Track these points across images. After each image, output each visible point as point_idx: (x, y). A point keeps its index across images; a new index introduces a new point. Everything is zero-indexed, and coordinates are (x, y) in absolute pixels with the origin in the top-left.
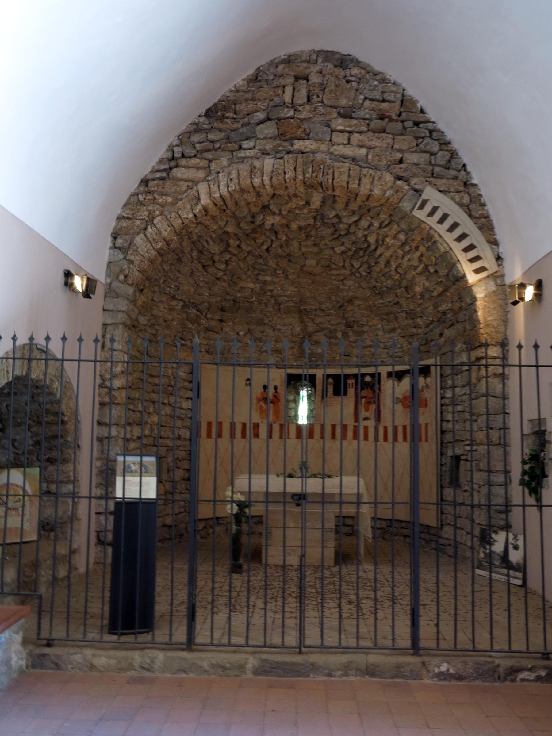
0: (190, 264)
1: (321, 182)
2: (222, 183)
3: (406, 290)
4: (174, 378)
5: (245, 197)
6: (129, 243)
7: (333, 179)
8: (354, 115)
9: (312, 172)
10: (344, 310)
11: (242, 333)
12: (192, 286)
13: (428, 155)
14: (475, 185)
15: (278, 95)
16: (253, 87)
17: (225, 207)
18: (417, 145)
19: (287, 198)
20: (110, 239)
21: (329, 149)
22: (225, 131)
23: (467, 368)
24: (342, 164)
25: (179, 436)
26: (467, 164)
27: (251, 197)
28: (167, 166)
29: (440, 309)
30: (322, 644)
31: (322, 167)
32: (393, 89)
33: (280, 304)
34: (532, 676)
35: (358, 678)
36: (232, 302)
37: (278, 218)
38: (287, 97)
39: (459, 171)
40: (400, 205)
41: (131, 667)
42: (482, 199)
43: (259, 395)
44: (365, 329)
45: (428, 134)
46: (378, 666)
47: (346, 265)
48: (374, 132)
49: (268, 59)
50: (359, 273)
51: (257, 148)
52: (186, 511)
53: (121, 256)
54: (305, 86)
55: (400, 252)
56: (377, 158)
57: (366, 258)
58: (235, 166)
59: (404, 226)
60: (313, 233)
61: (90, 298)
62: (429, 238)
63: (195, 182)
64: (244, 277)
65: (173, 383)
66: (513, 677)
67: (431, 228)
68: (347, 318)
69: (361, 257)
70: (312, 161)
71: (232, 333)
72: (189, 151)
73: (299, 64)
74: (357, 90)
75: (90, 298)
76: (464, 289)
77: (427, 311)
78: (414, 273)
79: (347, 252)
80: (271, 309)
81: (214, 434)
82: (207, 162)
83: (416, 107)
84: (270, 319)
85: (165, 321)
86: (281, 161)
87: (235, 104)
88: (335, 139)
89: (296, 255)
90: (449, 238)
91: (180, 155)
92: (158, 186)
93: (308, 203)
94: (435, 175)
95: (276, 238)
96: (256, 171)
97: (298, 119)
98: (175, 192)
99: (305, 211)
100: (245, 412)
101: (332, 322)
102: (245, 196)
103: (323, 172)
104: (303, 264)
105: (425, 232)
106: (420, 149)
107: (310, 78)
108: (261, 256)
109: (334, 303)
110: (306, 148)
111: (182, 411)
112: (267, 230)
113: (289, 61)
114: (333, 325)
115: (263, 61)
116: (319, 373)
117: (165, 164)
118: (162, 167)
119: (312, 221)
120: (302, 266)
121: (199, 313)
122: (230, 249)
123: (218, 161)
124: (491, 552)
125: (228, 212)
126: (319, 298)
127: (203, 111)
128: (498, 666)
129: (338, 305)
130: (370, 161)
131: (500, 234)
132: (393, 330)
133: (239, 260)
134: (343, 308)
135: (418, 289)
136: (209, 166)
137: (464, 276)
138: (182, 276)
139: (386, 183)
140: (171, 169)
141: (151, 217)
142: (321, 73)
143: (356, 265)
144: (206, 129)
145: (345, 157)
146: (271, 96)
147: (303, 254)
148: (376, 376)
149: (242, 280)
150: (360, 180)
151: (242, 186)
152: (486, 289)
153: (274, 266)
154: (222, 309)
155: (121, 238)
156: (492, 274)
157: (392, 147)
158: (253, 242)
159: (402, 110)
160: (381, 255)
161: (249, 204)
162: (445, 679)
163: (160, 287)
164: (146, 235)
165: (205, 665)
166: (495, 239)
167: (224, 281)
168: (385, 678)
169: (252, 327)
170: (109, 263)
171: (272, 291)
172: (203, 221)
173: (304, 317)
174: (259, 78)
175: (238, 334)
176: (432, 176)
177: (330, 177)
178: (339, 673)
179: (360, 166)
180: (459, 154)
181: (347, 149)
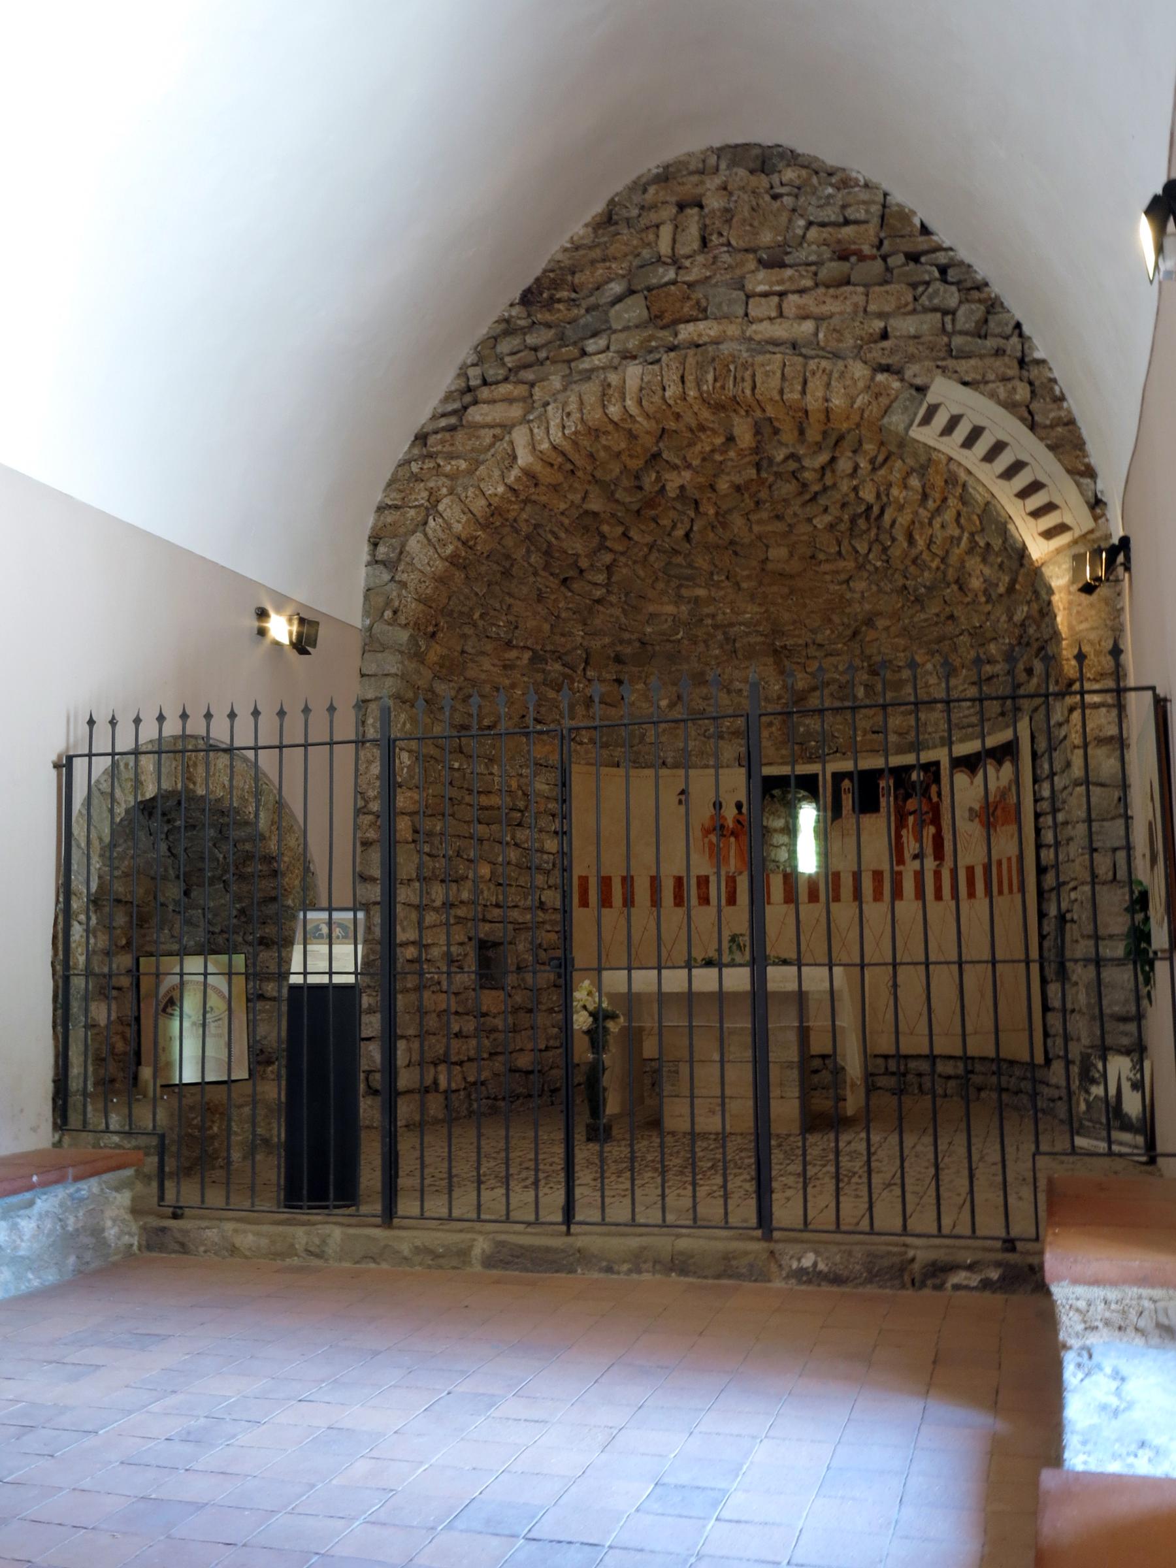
0: (532, 579)
1: (735, 397)
2: (552, 423)
4: (525, 794)
7: (754, 388)
8: (788, 260)
9: (715, 380)
12: (546, 620)
13: (939, 315)
15: (649, 244)
16: (603, 235)
17: (569, 467)
18: (915, 299)
20: (366, 548)
21: (743, 332)
22: (557, 326)
24: (768, 356)
25: (541, 903)
26: (1021, 321)
28: (457, 405)
32: (864, 195)
33: (735, 641)
34: (974, 1280)
35: (658, 1276)
36: (637, 644)
37: (687, 475)
38: (664, 247)
39: (1007, 338)
40: (885, 420)
41: (291, 1251)
42: (1057, 389)
43: (707, 823)
45: (937, 274)
46: (692, 1257)
47: (843, 552)
48: (828, 287)
49: (628, 180)
51: (612, 348)
53: (386, 577)
54: (696, 218)
58: (575, 387)
59: (910, 462)
60: (763, 494)
61: (308, 653)
62: (951, 480)
63: (507, 428)
65: (521, 804)
66: (938, 1281)
67: (950, 459)
68: (870, 657)
69: (865, 532)
70: (713, 360)
72: (494, 372)
73: (684, 180)
74: (794, 210)
75: (308, 653)
80: (717, 652)
82: (526, 387)
83: (911, 224)
84: (719, 671)
86: (656, 367)
87: (573, 273)
88: (753, 313)
91: (479, 382)
93: (731, 439)
94: (954, 353)
96: (611, 392)
97: (684, 283)
98: (472, 450)
99: (732, 454)
100: (681, 855)
102: (603, 440)
103: (735, 378)
104: (763, 557)
106: (923, 306)
107: (704, 202)
108: (676, 552)
109: (841, 628)
110: (700, 335)
111: (545, 857)
112: (674, 499)
113: (665, 177)
115: (618, 185)
117: (454, 400)
119: (753, 472)
122: (608, 544)
123: (545, 383)
125: (580, 474)
126: (807, 621)
127: (516, 295)
128: (913, 1260)
129: (849, 632)
130: (822, 344)
133: (635, 562)
134: (859, 638)
135: (976, 583)
136: (531, 395)
138: (518, 602)
139: (855, 382)
140: (465, 408)
141: (433, 499)
142: (725, 189)
143: (862, 548)
144: (522, 328)
145: (776, 343)
146: (636, 247)
147: (759, 537)
148: (932, 769)
151: (590, 424)
153: (705, 566)
154: (618, 659)
156: (1084, 536)
157: (865, 311)
158: (653, 525)
159: (882, 235)
160: (894, 522)
161: (618, 454)
162: (809, 1282)
163: (475, 625)
164: (426, 535)
165: (405, 1248)
168: (705, 1277)
170: (368, 590)
171: (713, 616)
172: (534, 497)
173: (786, 663)
174: (615, 217)
176: (947, 356)
178: (625, 1267)
179: (805, 357)
180: (1006, 304)
181: (776, 327)
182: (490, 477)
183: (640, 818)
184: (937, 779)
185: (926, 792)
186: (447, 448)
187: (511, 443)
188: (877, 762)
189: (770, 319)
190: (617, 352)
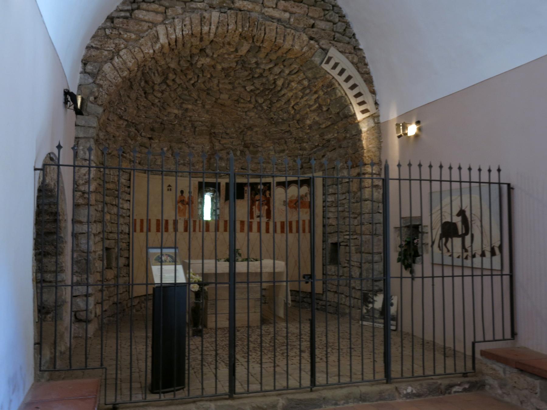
2: (177, 27)
3: (297, 122)
5: (192, 40)
6: (98, 69)
7: (265, 34)
10: (244, 134)
11: (165, 149)
14: (361, 50)
18: (324, 15)
19: (222, 45)
20: (80, 65)
21: (261, 10)
23: (347, 180)
24: (271, 23)
27: (196, 41)
28: (129, 8)
29: (326, 137)
30: (327, 383)
31: (256, 23)
35: (355, 404)
39: (350, 38)
40: (313, 59)
42: (366, 61)
44: (260, 149)
45: (331, 8)
50: (262, 107)
52: (126, 291)
55: (300, 94)
56: (297, 21)
57: (270, 96)
58: (188, 14)
60: (232, 74)
63: (155, 24)
64: (172, 104)
67: (333, 78)
70: (249, 18)
71: (158, 149)
76: (352, 124)
77: (314, 138)
78: (308, 110)
79: (255, 90)
81: (145, 229)
84: (187, 139)
85: (114, 137)
86: (226, 15)
89: (215, 90)
90: (346, 86)
92: (123, 23)
93: (236, 51)
95: (203, 76)
96: (205, 20)
98: (138, 30)
99: (232, 56)
101: (234, 144)
105: (328, 81)
106: (326, 18)
111: (124, 211)
112: (197, 68)
114: (235, 145)
116: (223, 182)
117: (128, 5)
118: (126, 8)
120: (217, 99)
121: (136, 132)
122: (168, 81)
123: (174, 9)
124: (373, 308)
128: (441, 384)
129: (240, 130)
131: (377, 86)
132: (283, 151)
134: (244, 133)
136: (165, 12)
137: (355, 114)
139: (303, 41)
140: (133, 10)
143: (261, 100)
148: (268, 186)
149: (170, 107)
150: (284, 37)
152: (368, 125)
153: (196, 97)
154: (152, 130)
155: (91, 65)
157: (307, 15)
158: (185, 77)
160: (284, 95)
162: (410, 398)
164: (113, 65)
166: (374, 90)
167: (157, 106)
168: (373, 402)
169: (173, 144)
170: (80, 85)
171: (190, 117)
175: (162, 149)
177: (263, 32)
178: (342, 402)
180: (351, 25)
182: (146, 45)
183: (152, 196)
184: (269, 189)
185: (264, 193)
186: (125, 27)
187: (157, 31)
188: (244, 180)
189: (272, 7)
190: (207, 4)
